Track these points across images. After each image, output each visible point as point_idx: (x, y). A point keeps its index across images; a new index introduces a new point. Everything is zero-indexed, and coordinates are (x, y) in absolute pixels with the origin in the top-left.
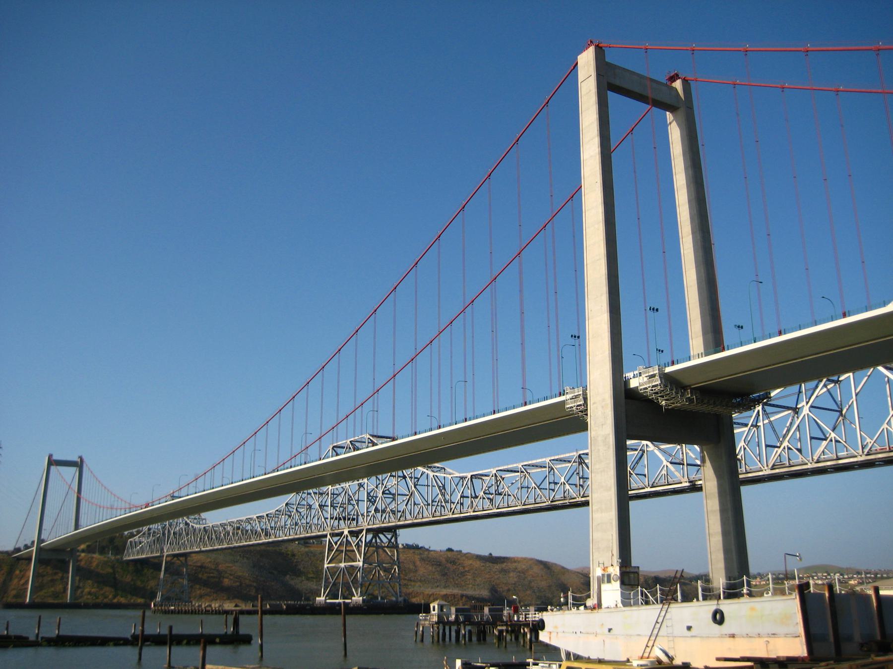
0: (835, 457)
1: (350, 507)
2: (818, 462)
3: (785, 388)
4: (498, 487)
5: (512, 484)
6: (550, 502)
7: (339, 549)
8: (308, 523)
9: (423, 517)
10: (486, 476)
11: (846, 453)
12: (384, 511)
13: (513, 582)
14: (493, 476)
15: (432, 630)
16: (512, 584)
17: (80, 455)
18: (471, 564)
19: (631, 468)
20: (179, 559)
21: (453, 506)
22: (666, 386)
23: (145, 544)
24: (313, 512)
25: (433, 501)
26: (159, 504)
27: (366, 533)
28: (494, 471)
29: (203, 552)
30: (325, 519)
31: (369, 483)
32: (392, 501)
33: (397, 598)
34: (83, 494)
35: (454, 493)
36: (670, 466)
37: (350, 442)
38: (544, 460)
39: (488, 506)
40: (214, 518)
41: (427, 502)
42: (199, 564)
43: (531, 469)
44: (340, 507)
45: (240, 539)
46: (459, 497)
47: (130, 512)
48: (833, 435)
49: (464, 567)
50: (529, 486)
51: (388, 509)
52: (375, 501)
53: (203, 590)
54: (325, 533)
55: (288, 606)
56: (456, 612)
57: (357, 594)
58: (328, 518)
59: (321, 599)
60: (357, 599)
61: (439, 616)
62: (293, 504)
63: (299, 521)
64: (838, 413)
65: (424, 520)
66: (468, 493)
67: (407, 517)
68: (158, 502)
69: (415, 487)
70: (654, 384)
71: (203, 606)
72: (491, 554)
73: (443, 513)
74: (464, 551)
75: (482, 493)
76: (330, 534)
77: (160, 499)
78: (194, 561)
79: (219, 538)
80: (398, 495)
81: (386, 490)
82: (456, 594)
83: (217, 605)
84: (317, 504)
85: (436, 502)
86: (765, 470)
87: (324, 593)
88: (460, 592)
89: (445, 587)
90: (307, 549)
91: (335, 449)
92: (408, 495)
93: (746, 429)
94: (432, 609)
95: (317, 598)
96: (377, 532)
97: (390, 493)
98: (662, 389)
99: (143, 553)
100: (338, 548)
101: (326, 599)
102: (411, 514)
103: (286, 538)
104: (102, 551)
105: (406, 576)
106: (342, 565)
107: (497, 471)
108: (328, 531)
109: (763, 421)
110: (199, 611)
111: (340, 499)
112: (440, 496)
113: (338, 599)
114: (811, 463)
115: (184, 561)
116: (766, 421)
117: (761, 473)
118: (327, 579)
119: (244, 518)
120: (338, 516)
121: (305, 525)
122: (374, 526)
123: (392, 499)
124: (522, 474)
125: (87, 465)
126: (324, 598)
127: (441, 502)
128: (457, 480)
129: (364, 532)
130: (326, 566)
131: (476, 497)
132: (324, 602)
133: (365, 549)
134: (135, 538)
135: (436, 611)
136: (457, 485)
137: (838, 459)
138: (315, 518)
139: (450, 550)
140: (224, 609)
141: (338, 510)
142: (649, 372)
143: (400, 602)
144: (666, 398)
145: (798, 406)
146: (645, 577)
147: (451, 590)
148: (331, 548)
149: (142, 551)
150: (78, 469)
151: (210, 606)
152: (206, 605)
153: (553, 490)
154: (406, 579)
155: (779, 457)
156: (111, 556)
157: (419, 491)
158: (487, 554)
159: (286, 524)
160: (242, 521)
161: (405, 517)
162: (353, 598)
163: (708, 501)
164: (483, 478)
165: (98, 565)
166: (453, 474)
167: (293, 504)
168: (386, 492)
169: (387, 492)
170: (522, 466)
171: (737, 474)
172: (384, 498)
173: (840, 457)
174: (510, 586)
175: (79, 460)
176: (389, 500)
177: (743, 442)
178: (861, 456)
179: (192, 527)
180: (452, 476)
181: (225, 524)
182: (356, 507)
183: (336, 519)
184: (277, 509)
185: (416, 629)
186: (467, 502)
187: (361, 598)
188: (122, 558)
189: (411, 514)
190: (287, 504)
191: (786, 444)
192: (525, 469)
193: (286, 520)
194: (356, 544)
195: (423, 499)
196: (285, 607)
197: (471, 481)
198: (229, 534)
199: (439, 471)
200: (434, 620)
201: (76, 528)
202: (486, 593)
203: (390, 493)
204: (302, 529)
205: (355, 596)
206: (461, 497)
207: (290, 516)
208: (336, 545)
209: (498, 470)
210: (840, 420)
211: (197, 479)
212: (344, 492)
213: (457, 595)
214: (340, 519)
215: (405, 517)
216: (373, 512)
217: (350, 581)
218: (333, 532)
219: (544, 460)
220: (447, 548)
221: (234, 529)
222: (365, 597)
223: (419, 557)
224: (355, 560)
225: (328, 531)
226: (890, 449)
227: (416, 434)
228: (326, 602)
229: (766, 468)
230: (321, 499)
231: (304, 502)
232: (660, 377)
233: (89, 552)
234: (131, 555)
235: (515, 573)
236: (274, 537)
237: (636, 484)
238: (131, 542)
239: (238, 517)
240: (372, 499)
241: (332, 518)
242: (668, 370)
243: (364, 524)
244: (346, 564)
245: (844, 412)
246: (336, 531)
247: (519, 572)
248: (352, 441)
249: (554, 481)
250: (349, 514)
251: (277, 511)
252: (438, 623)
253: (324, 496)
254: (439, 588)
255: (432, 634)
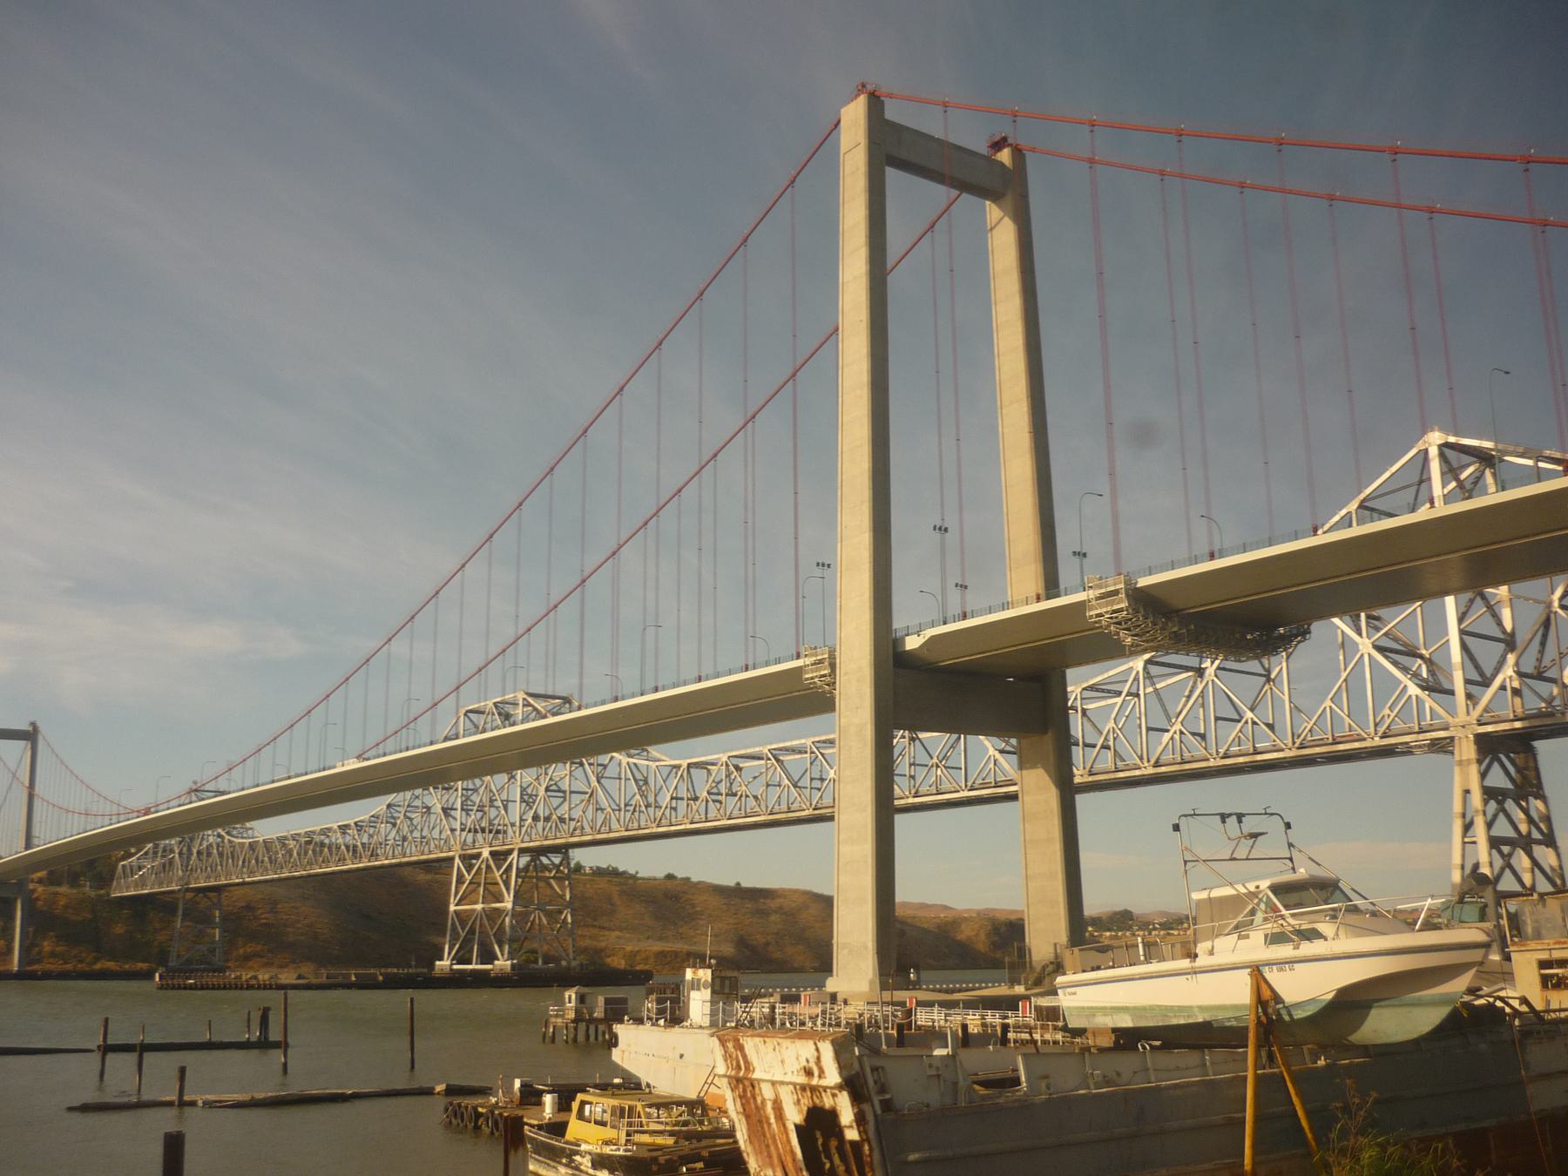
0: (1251, 751)
1: (493, 813)
2: (1226, 756)
3: (1424, 602)
4: (731, 784)
5: (755, 778)
6: (811, 810)
7: (474, 881)
8: (424, 838)
9: (610, 831)
10: (713, 764)
11: (1238, 748)
12: (547, 819)
13: (776, 931)
14: (722, 765)
15: (565, 1032)
16: (773, 934)
17: (32, 720)
18: (706, 900)
19: (940, 758)
20: (205, 896)
21: (659, 814)
22: (1136, 611)
23: (148, 869)
24: (433, 817)
25: (626, 805)
26: (168, 809)
27: (519, 856)
28: (725, 759)
29: (249, 883)
30: (453, 830)
31: (525, 776)
32: (563, 802)
33: (569, 963)
34: (38, 790)
35: (661, 793)
36: (998, 756)
37: (495, 704)
38: (803, 741)
39: (714, 815)
40: (266, 829)
41: (618, 806)
42: (243, 904)
43: (825, 748)
44: (477, 811)
45: (326, 862)
46: (668, 798)
47: (119, 822)
48: (1249, 715)
49: (693, 906)
50: (824, 777)
51: (554, 817)
52: (534, 802)
53: (250, 947)
54: (451, 854)
55: (386, 976)
56: (606, 1004)
57: (503, 955)
58: (455, 830)
59: (444, 964)
60: (503, 963)
61: (577, 1011)
62: (399, 806)
63: (409, 834)
64: (1264, 679)
65: (612, 835)
66: (683, 793)
67: (612, 827)
68: (165, 806)
69: (599, 782)
70: (1115, 607)
71: (244, 978)
72: (738, 884)
73: (673, 820)
74: (695, 879)
75: (705, 794)
76: (460, 856)
77: (168, 801)
78: (234, 899)
79: (276, 861)
80: (571, 792)
81: (551, 785)
82: (679, 950)
83: (267, 977)
84: (439, 806)
85: (631, 805)
86: (1145, 768)
87: (449, 953)
88: (686, 947)
89: (661, 939)
90: (429, 877)
91: (469, 714)
92: (586, 793)
93: (1119, 700)
94: (567, 1000)
95: (438, 963)
96: (537, 852)
97: (559, 791)
98: (1130, 616)
99: (143, 886)
100: (472, 878)
101: (452, 964)
102: (618, 821)
103: (386, 862)
104: (74, 880)
105: (595, 920)
106: (479, 907)
107: (729, 757)
108: (455, 853)
109: (1144, 688)
110: (236, 985)
111: (476, 798)
112: (638, 797)
113: (470, 963)
114: (1214, 759)
115: (215, 901)
116: (1150, 690)
117: (1137, 773)
118: (454, 928)
119: (318, 828)
120: (472, 826)
121: (419, 840)
122: (532, 844)
123: (562, 799)
124: (769, 762)
125: (44, 738)
126: (448, 963)
127: (640, 806)
128: (665, 772)
129: (515, 853)
130: (452, 908)
131: (696, 799)
132: (448, 968)
133: (516, 882)
134: (130, 860)
135: (573, 1004)
136: (667, 778)
137: (1256, 752)
138: (435, 830)
139: (670, 877)
140: (279, 981)
141: (473, 817)
142: (1107, 586)
143: (575, 968)
144: (1126, 626)
145: (1203, 666)
146: (994, 924)
147: (670, 945)
148: (460, 880)
149: (142, 882)
150: (29, 746)
151: (255, 977)
152: (249, 976)
153: (819, 789)
154: (595, 926)
155: (1171, 742)
156: (88, 890)
157: (606, 790)
158: (732, 883)
159: (388, 838)
160: (314, 832)
161: (610, 827)
162: (496, 962)
163: (1026, 826)
164: (709, 767)
165: (66, 907)
166: (659, 760)
167: (399, 806)
168: (551, 788)
169: (554, 788)
170: (769, 750)
171: (1072, 775)
172: (549, 797)
173: (1259, 750)
174: (769, 938)
175: (31, 729)
176: (556, 802)
177: (1113, 721)
178: (1290, 749)
179: (230, 841)
180: (657, 763)
181: (285, 838)
182: (503, 812)
183: (470, 831)
184: (372, 814)
185: (544, 1030)
186: (682, 805)
187: (509, 962)
188: (108, 894)
189: (618, 821)
190: (389, 806)
191: (1178, 727)
192: (817, 748)
193: (388, 831)
194: (503, 873)
195: (611, 801)
196: (381, 978)
197: (689, 772)
198: (291, 856)
199: (638, 754)
200: (570, 1017)
201: (28, 847)
202: (729, 949)
203: (559, 791)
204: (414, 848)
205: (498, 960)
206: (672, 798)
207: (394, 825)
208: (469, 875)
209: (732, 757)
210: (1267, 690)
211: (230, 769)
212: (484, 786)
213: (681, 952)
214: (476, 831)
215: (610, 827)
216: (530, 820)
217: (491, 933)
218: (464, 852)
219: (803, 741)
220: (666, 873)
221: (300, 846)
222: (515, 961)
223: (618, 888)
224: (501, 900)
225: (455, 853)
226: (1334, 739)
227: (700, 679)
228: (451, 970)
229: (1146, 764)
230: (446, 797)
231: (417, 803)
232: (1127, 595)
233: (52, 884)
234: (123, 889)
235: (778, 916)
236: (367, 860)
237: (902, 793)
238: (124, 866)
239: (308, 827)
240: (528, 799)
241: (462, 830)
242: (1143, 582)
243: (515, 840)
244: (486, 906)
245: (1273, 676)
246: (469, 852)
247: (784, 913)
248: (498, 702)
249: (821, 775)
250: (491, 824)
251: (373, 816)
252: (575, 1021)
253: (451, 791)
254: (650, 941)
255: (565, 1038)
